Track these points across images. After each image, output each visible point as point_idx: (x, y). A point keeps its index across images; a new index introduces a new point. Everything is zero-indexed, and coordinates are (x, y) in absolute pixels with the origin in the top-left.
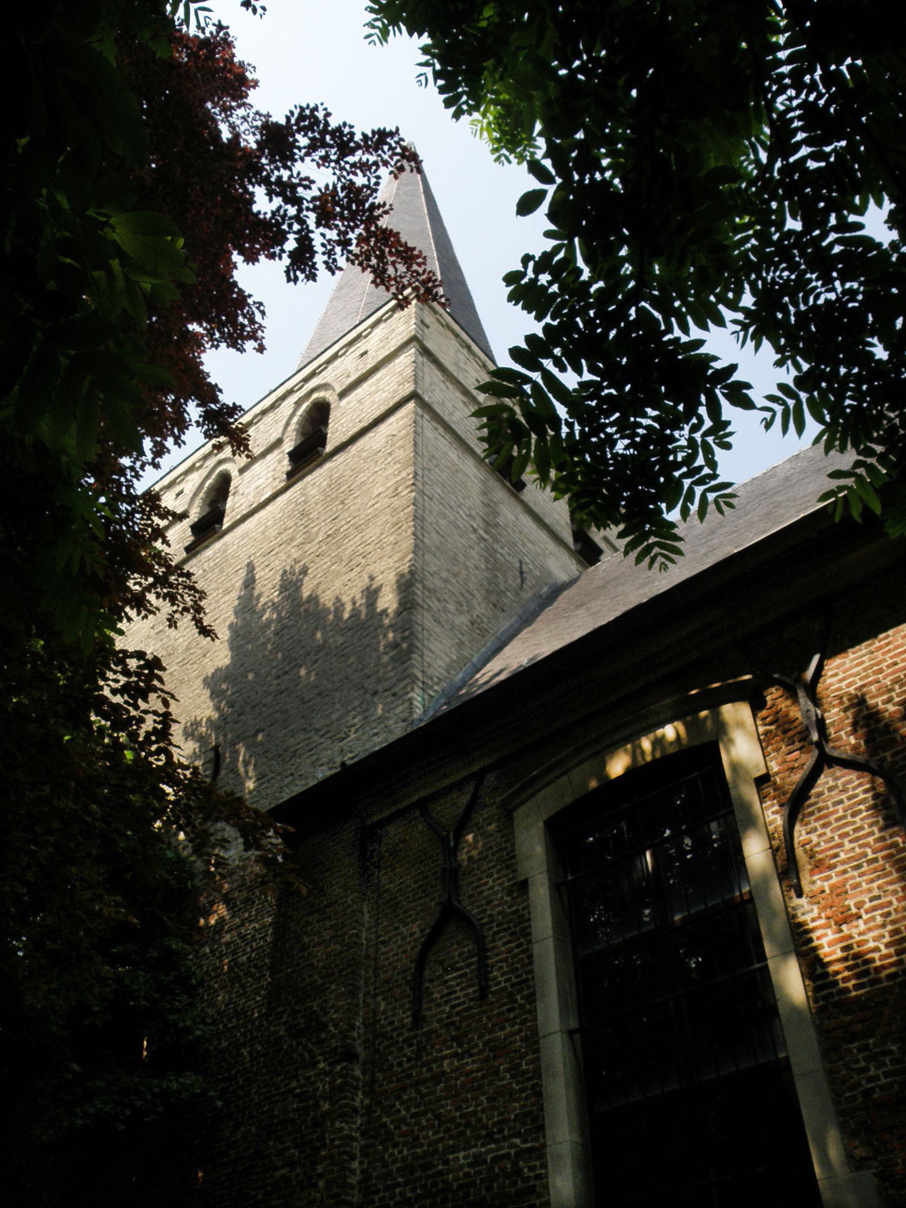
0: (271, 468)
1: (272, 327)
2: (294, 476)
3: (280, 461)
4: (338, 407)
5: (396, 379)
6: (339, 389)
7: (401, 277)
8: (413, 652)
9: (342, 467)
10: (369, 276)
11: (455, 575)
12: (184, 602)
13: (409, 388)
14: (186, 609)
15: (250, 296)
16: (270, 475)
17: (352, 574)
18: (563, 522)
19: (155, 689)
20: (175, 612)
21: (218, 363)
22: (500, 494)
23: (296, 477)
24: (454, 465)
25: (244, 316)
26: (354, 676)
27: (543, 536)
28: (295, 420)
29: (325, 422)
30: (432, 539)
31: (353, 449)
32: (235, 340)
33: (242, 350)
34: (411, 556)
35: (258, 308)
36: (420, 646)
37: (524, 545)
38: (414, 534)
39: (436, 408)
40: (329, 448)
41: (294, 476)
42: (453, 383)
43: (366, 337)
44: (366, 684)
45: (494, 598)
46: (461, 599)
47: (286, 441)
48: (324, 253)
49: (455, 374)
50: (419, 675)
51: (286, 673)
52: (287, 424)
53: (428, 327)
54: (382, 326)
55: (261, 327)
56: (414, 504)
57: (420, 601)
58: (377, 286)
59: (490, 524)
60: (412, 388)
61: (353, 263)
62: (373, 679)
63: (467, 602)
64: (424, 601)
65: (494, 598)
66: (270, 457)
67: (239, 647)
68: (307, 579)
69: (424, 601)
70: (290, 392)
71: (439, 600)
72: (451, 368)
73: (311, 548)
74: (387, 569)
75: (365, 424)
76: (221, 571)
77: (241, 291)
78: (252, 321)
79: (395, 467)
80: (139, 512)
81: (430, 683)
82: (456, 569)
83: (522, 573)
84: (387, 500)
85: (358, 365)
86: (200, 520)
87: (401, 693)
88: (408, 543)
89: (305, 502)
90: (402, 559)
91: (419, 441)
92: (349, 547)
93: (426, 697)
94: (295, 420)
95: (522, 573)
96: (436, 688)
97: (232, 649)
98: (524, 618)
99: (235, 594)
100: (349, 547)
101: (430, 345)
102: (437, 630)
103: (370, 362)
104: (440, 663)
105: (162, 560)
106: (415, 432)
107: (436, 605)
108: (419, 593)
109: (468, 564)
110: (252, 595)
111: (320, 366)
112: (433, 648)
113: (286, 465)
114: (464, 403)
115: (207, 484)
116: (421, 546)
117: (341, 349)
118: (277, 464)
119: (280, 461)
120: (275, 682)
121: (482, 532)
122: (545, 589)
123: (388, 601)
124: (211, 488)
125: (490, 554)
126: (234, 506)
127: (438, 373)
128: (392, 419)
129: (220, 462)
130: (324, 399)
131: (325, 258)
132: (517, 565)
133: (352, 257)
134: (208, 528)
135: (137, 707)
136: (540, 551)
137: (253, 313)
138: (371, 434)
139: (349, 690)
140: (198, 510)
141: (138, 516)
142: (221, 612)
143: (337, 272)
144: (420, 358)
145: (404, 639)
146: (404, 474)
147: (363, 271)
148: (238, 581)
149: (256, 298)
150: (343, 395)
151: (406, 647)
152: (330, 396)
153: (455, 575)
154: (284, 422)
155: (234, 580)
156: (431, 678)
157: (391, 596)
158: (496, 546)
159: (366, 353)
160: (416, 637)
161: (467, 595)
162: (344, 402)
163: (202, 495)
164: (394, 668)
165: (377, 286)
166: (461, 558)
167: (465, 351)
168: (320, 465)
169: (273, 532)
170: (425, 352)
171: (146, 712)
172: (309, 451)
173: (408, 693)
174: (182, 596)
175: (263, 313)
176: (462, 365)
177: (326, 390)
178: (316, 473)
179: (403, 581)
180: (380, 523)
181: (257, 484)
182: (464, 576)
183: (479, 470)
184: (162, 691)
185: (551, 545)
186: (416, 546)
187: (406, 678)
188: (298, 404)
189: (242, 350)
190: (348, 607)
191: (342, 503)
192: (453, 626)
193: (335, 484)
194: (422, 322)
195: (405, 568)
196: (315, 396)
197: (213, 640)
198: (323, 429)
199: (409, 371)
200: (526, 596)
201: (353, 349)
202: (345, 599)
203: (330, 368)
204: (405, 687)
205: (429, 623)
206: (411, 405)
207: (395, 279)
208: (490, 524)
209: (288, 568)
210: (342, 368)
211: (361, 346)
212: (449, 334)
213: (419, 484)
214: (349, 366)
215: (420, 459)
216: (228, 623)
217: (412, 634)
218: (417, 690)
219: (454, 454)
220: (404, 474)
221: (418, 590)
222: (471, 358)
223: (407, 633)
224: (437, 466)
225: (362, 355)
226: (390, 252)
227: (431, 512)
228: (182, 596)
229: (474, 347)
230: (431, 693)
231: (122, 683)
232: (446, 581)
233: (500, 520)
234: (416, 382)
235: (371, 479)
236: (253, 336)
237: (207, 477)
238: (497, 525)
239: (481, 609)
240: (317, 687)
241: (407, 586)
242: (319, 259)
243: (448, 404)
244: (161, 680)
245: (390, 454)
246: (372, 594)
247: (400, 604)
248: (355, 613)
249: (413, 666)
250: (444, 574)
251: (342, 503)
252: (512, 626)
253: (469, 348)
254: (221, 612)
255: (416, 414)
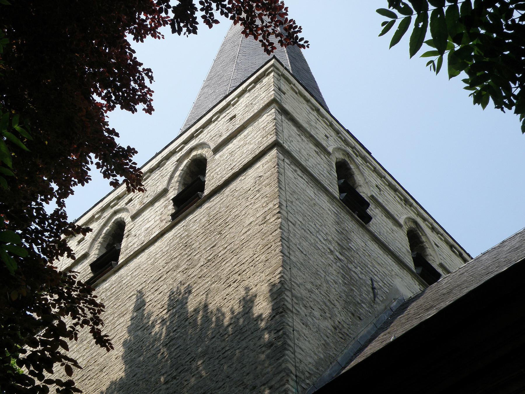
0: (159, 212)
1: (159, 88)
2: (177, 217)
3: (166, 207)
4: (213, 160)
5: (259, 134)
6: (213, 146)
7: (267, 26)
8: (286, 349)
9: (218, 206)
10: (240, 27)
11: (318, 287)
12: (85, 315)
13: (272, 139)
14: (86, 322)
15: (141, 64)
16: (157, 218)
17: (230, 290)
18: (404, 250)
19: (59, 358)
20: (76, 324)
21: (117, 119)
22: (350, 224)
23: (180, 217)
24: (312, 199)
25: (136, 82)
26: (235, 375)
27: (389, 260)
28: (178, 173)
29: (203, 172)
30: (296, 257)
31: (227, 191)
32: (129, 105)
33: (134, 110)
34: (281, 269)
35: (147, 74)
36: (292, 345)
37: (374, 267)
38: (281, 252)
39: (294, 154)
40: (206, 192)
41: (177, 217)
42: (306, 137)
43: (233, 105)
44: (245, 381)
45: (352, 308)
46: (324, 307)
47: (171, 190)
48: (202, 10)
49: (308, 130)
50: (293, 369)
51: (174, 378)
52: (171, 177)
53: (284, 94)
54: (247, 95)
55: (150, 92)
56: (280, 228)
57: (290, 307)
58: (247, 35)
59: (344, 247)
60: (274, 139)
61: (227, 16)
62: (251, 376)
63: (329, 310)
64: (293, 306)
65: (352, 308)
66: (157, 204)
67: (132, 360)
68: (191, 297)
69: (293, 306)
70: (173, 153)
71: (305, 307)
72: (305, 125)
73: (195, 272)
74: (260, 284)
75: (236, 169)
76: (117, 299)
77: (134, 61)
78: (143, 86)
79: (263, 201)
80: (47, 231)
81: (303, 377)
82: (319, 282)
83: (373, 289)
84: (257, 227)
85: (228, 126)
86: (98, 259)
87: (277, 386)
88: (277, 260)
89: (188, 236)
90: (273, 272)
91: (282, 178)
92: (227, 268)
93: (299, 389)
94: (178, 173)
95: (373, 289)
96: (308, 381)
97: (126, 363)
98: (379, 326)
99: (128, 316)
100: (227, 268)
101: (287, 107)
102: (306, 331)
103: (238, 123)
104: (310, 360)
105: (65, 278)
106: (278, 172)
107: (303, 311)
108: (289, 300)
109: (328, 278)
110: (143, 315)
111: (197, 131)
112: (303, 347)
113: (171, 209)
114: (317, 153)
115: (104, 231)
116: (288, 261)
117: (214, 115)
118: (165, 208)
119: (166, 207)
120: (165, 387)
121: (337, 254)
122: (395, 304)
123: (263, 307)
124: (108, 234)
125: (346, 273)
126: (128, 245)
127: (295, 129)
128: (259, 164)
129: (116, 213)
130: (201, 155)
131: (204, 13)
132: (369, 282)
133: (225, 11)
134: (107, 263)
135: (41, 377)
136: (387, 272)
137: (143, 78)
138: (241, 178)
139: (231, 387)
140: (97, 252)
141: (47, 234)
142: (117, 325)
143: (214, 24)
144: (280, 117)
145: (278, 338)
146: (271, 205)
147: (235, 23)
148: (131, 305)
149: (145, 66)
150: (216, 150)
151: (279, 347)
152: (206, 152)
153: (318, 287)
154: (168, 176)
155: (128, 305)
156: (303, 373)
157: (265, 304)
158: (350, 266)
159: (234, 116)
160: (288, 336)
161: (328, 304)
162: (217, 156)
163: (100, 240)
164: (270, 365)
165: (247, 35)
166: (323, 274)
167: (315, 113)
168: (200, 205)
169: (161, 262)
170: (283, 111)
171: (50, 382)
172: (191, 194)
173: (284, 385)
174: (83, 310)
175: (151, 78)
176: (313, 124)
177: (203, 148)
178: (197, 213)
179: (275, 289)
180: (252, 246)
181: (147, 226)
182: (325, 288)
183: (332, 205)
184: (66, 358)
185: (396, 268)
186: (284, 261)
187: (280, 372)
188: (180, 161)
189: (134, 110)
190: (228, 316)
191: (220, 233)
192: (319, 330)
193: (212, 220)
194: (279, 89)
195: (276, 279)
196: (194, 153)
197: (108, 350)
198: (201, 178)
199: (271, 126)
200: (379, 307)
201: (224, 115)
202: (224, 310)
203: (206, 131)
204: (281, 379)
205: (298, 325)
206: (274, 152)
207: (262, 29)
208: (344, 247)
209: (175, 290)
210: (216, 130)
211: (231, 112)
212: (302, 99)
213: (284, 213)
214: (221, 128)
215: (283, 193)
216: (122, 341)
217: (284, 334)
218: (292, 383)
219: (311, 191)
220: (271, 205)
221: (288, 297)
222: (320, 119)
223: (281, 333)
224: (298, 199)
225: (231, 119)
226: (257, 6)
227: (295, 235)
228: (83, 310)
229: (322, 110)
230: (303, 385)
231: (29, 353)
232: (310, 291)
233: (352, 245)
234: (277, 134)
235: (243, 213)
236: (144, 99)
237: (105, 225)
238: (349, 249)
239: (341, 317)
240: (201, 388)
241: (278, 293)
242: (199, 15)
243: (304, 153)
244: (66, 347)
245: (258, 191)
246: (248, 302)
247: (273, 310)
248: (235, 319)
249: (287, 361)
250: (309, 286)
251: (220, 233)
252: (368, 332)
253: (318, 111)
254: (117, 325)
255: (279, 159)
